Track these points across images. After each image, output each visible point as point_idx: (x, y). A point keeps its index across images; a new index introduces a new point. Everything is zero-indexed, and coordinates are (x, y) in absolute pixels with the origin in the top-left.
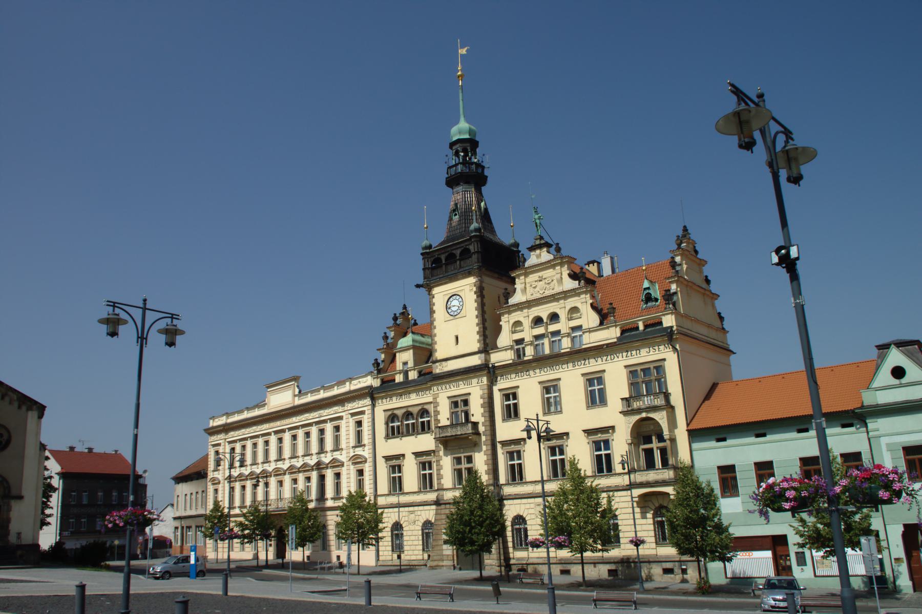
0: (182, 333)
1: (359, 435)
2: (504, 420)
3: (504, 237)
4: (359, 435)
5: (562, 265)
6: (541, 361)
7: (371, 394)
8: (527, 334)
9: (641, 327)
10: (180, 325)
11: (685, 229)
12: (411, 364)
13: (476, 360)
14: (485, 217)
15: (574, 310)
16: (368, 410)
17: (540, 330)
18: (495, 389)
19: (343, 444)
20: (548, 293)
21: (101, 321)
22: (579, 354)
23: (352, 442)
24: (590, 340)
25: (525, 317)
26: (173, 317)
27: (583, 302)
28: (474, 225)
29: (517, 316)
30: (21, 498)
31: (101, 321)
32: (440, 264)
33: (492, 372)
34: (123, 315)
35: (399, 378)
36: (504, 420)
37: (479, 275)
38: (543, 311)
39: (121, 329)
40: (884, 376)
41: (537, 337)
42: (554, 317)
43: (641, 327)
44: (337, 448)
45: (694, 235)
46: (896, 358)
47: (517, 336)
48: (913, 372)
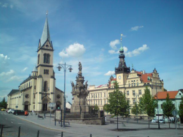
0: (72, 69)
1: (105, 95)
2: (132, 90)
3: (128, 66)
4: (105, 95)
5: (136, 73)
6: (132, 87)
7: (107, 89)
8: (131, 83)
9: (147, 84)
10: (72, 68)
11: (155, 69)
12: (113, 85)
13: (123, 86)
14: (125, 63)
15: (137, 80)
16: (106, 92)
17: (132, 83)
18: (126, 91)
19: (102, 96)
20: (134, 77)
21: (57, 68)
22: (138, 87)
23: (104, 96)
24: (140, 85)
25: (131, 80)
26: (71, 66)
27: (139, 79)
28: (123, 66)
29: (129, 80)
30: (62, 104)
31: (57, 68)
32: (118, 71)
33: (125, 88)
34: (61, 66)
35: (111, 88)
36: (132, 90)
37: (123, 73)
38: (133, 80)
39: (61, 69)
40: (178, 94)
41: (132, 84)
42: (134, 81)
43: (147, 84)
44: (101, 97)
45: (156, 69)
46: (180, 92)
47: (129, 83)
48: (182, 94)
